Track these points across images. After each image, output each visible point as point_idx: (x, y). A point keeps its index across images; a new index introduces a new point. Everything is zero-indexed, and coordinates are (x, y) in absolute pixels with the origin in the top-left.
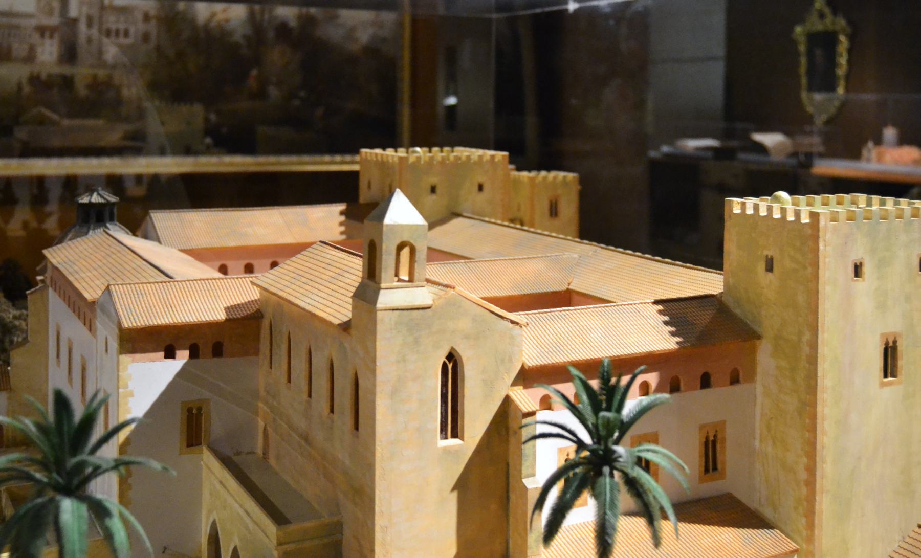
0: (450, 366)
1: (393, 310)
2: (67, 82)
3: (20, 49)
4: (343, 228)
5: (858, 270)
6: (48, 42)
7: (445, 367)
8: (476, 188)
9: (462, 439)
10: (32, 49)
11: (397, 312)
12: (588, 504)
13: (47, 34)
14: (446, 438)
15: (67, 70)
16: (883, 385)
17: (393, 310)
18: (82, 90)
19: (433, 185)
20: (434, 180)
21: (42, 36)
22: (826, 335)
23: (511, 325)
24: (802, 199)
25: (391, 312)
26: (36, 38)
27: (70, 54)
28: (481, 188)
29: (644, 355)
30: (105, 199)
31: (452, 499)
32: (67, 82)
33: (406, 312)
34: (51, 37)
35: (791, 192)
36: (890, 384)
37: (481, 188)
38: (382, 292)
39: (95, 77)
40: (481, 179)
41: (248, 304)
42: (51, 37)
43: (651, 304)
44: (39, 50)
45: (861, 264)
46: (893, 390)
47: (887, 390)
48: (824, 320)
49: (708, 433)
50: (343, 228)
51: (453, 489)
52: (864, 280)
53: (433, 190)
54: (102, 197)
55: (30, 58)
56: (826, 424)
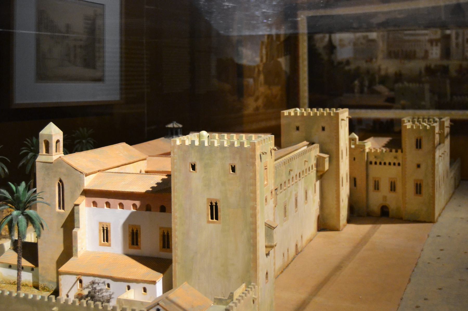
0: (61, 184)
1: (41, 162)
2: (445, 69)
3: (420, 54)
4: (394, 150)
5: (194, 167)
6: (434, 48)
7: (59, 183)
8: (321, 129)
9: (64, 210)
10: (426, 52)
11: (42, 163)
12: (129, 249)
13: (434, 44)
14: (61, 209)
15: (445, 62)
16: (209, 222)
17: (41, 162)
18: (453, 72)
19: (298, 126)
20: (298, 124)
21: (432, 44)
22: (176, 194)
23: (80, 173)
24: (216, 135)
25: (40, 163)
26: (428, 46)
27: (446, 54)
28: (323, 129)
29: (140, 193)
30: (178, 126)
31: (62, 230)
32: (445, 69)
33: (45, 163)
34: (437, 45)
35: (208, 131)
36: (214, 223)
37: (323, 129)
38: (39, 156)
39: (461, 66)
40: (323, 124)
41: (393, 190)
42: (437, 45)
43: (165, 176)
44: (430, 52)
45: (195, 164)
46: (214, 226)
47: (211, 225)
48: (175, 187)
49: (164, 231)
50: (394, 150)
51: (62, 227)
52: (196, 172)
53: (298, 129)
54: (177, 125)
55: (426, 56)
56: (177, 233)
